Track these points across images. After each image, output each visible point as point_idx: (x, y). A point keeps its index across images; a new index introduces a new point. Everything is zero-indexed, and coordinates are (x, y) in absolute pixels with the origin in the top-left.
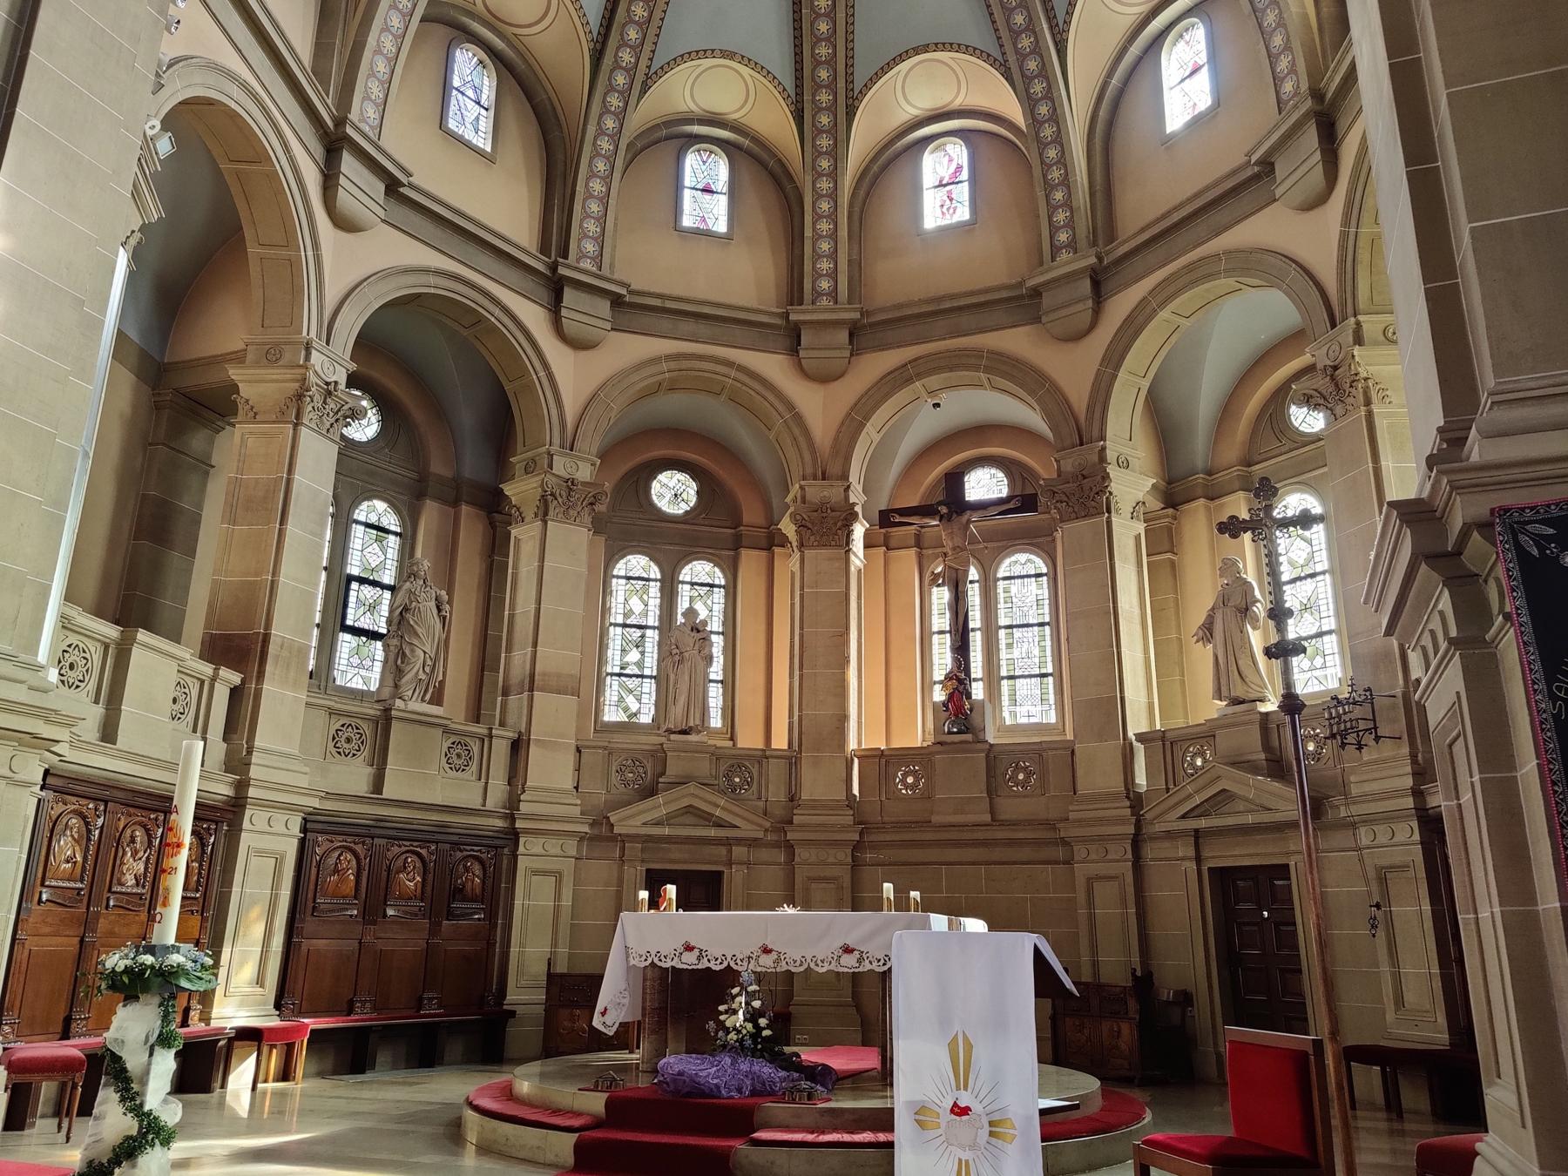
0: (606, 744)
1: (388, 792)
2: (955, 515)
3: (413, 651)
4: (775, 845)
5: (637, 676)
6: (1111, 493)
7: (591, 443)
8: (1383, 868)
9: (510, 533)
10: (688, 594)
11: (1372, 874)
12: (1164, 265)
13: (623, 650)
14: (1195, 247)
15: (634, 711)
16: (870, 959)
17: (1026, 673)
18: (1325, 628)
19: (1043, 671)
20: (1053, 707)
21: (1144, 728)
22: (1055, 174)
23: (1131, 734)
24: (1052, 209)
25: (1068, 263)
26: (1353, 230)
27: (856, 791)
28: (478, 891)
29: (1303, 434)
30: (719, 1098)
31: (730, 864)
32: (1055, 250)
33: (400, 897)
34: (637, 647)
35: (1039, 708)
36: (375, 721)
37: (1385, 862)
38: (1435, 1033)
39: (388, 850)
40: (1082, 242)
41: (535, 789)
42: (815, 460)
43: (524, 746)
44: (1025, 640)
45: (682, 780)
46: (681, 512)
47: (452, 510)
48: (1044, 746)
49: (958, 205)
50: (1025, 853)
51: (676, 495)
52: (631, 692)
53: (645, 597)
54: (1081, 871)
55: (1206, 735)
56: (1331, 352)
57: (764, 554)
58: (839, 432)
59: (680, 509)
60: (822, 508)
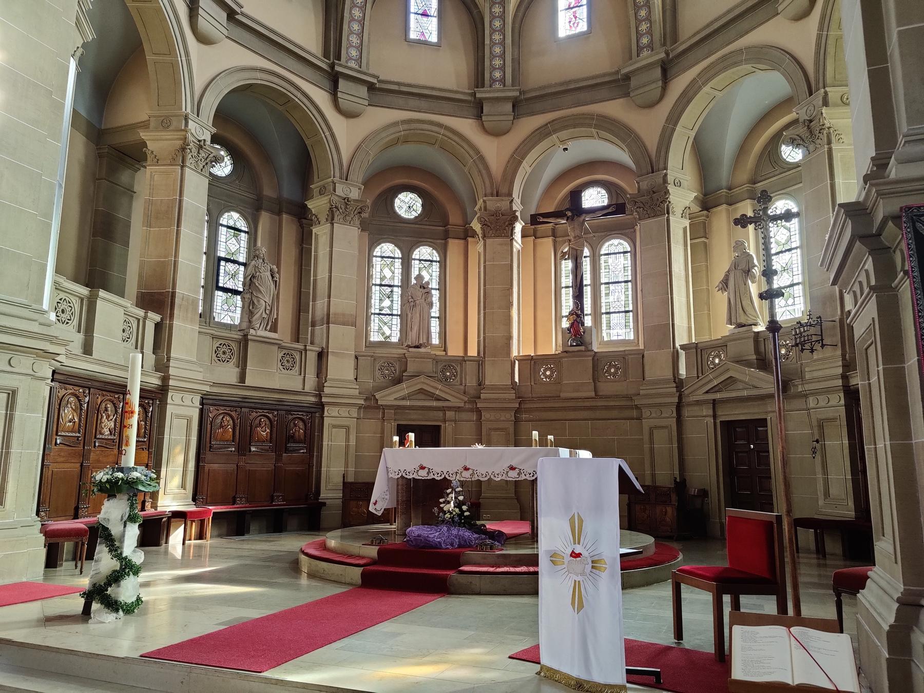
1: (248, 382)
3: (258, 301)
4: (471, 410)
6: (670, 202)
7: (358, 176)
10: (418, 266)
11: (815, 423)
12: (707, 57)
14: (727, 45)
16: (525, 473)
17: (617, 310)
18: (795, 282)
19: (627, 309)
20: (632, 330)
21: (685, 342)
23: (677, 345)
24: (638, 22)
27: (517, 380)
28: (302, 437)
31: (445, 421)
32: (640, 49)
33: (258, 441)
34: (389, 298)
35: (624, 330)
46: (413, 217)
47: (277, 217)
49: (580, 21)
50: (615, 413)
51: (409, 207)
52: (385, 324)
53: (393, 268)
54: (647, 424)
55: (721, 345)
56: (808, 111)
57: (462, 242)
58: (507, 166)
59: (412, 215)
60: (496, 214)
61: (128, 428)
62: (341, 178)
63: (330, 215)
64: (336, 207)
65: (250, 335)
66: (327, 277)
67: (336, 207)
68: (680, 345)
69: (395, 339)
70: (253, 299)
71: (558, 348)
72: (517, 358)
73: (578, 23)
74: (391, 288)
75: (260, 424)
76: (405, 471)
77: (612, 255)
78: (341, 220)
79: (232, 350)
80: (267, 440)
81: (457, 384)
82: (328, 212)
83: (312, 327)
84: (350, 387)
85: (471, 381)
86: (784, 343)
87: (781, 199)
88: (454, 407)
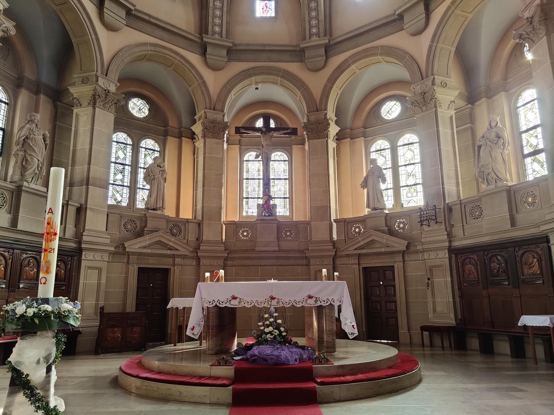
0: (120, 212)
1: (20, 227)
2: (267, 132)
3: (32, 159)
4: (192, 258)
5: (121, 186)
6: (329, 131)
7: (114, 75)
8: (431, 266)
9: (73, 111)
10: (144, 152)
11: (428, 269)
12: (355, 48)
13: (115, 174)
14: (368, 43)
15: (119, 200)
16: (320, 300)
17: (279, 197)
18: (389, 187)
19: (285, 196)
20: (288, 210)
21: (335, 218)
23: (332, 220)
24: (310, 19)
25: (316, 41)
26: (435, 44)
27: (224, 238)
28: (63, 277)
29: (386, 120)
30: (290, 365)
31: (174, 265)
32: (311, 35)
33: (26, 279)
34: (121, 173)
35: (283, 210)
36: (12, 192)
37: (433, 264)
39: (21, 256)
40: (322, 34)
41: (89, 230)
42: (210, 102)
43: (84, 210)
44: (279, 184)
45: (155, 230)
46: (142, 117)
47: (35, 97)
48: (299, 222)
49: (269, 10)
51: (140, 109)
52: (118, 192)
53: (125, 152)
55: (362, 220)
56: (422, 88)
57: (177, 140)
58: (221, 91)
59: (141, 115)
60: (214, 122)
61: (49, 252)
62: (102, 73)
63: (93, 101)
64: (99, 95)
65: (24, 186)
66: (88, 148)
67: (99, 95)
68: (333, 220)
69: (124, 204)
70: (27, 156)
71: (241, 218)
72: (225, 222)
73: (268, 11)
74: (124, 166)
75: (29, 264)
76: (219, 301)
77: (277, 162)
78: (102, 106)
79: (4, 198)
80: (34, 278)
81: (181, 238)
82: (90, 98)
83: (70, 187)
84: (104, 236)
85: (192, 237)
86: (358, 226)
87: (382, 139)
88: (182, 255)
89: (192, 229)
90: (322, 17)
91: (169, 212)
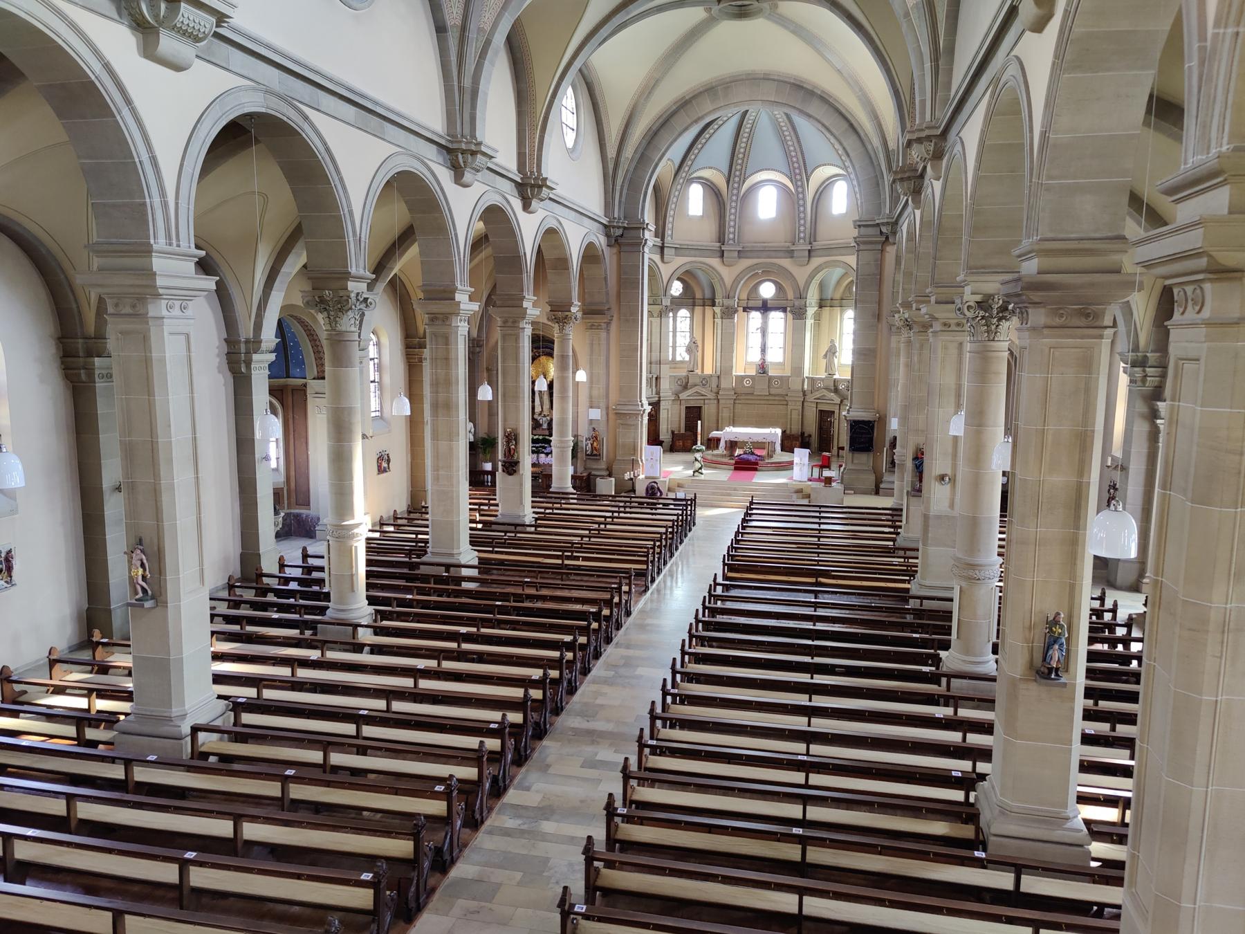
22: (802, 209)
38: (87, 707)
50: (776, 402)
54: (790, 407)
85: (714, 386)
89: (714, 381)
90: (808, 225)
91: (698, 371)
